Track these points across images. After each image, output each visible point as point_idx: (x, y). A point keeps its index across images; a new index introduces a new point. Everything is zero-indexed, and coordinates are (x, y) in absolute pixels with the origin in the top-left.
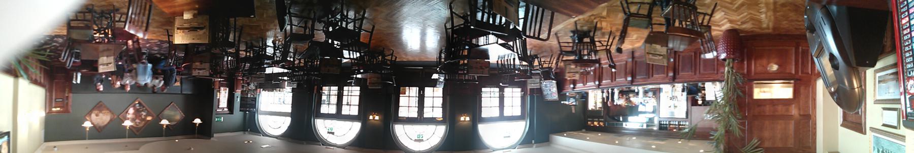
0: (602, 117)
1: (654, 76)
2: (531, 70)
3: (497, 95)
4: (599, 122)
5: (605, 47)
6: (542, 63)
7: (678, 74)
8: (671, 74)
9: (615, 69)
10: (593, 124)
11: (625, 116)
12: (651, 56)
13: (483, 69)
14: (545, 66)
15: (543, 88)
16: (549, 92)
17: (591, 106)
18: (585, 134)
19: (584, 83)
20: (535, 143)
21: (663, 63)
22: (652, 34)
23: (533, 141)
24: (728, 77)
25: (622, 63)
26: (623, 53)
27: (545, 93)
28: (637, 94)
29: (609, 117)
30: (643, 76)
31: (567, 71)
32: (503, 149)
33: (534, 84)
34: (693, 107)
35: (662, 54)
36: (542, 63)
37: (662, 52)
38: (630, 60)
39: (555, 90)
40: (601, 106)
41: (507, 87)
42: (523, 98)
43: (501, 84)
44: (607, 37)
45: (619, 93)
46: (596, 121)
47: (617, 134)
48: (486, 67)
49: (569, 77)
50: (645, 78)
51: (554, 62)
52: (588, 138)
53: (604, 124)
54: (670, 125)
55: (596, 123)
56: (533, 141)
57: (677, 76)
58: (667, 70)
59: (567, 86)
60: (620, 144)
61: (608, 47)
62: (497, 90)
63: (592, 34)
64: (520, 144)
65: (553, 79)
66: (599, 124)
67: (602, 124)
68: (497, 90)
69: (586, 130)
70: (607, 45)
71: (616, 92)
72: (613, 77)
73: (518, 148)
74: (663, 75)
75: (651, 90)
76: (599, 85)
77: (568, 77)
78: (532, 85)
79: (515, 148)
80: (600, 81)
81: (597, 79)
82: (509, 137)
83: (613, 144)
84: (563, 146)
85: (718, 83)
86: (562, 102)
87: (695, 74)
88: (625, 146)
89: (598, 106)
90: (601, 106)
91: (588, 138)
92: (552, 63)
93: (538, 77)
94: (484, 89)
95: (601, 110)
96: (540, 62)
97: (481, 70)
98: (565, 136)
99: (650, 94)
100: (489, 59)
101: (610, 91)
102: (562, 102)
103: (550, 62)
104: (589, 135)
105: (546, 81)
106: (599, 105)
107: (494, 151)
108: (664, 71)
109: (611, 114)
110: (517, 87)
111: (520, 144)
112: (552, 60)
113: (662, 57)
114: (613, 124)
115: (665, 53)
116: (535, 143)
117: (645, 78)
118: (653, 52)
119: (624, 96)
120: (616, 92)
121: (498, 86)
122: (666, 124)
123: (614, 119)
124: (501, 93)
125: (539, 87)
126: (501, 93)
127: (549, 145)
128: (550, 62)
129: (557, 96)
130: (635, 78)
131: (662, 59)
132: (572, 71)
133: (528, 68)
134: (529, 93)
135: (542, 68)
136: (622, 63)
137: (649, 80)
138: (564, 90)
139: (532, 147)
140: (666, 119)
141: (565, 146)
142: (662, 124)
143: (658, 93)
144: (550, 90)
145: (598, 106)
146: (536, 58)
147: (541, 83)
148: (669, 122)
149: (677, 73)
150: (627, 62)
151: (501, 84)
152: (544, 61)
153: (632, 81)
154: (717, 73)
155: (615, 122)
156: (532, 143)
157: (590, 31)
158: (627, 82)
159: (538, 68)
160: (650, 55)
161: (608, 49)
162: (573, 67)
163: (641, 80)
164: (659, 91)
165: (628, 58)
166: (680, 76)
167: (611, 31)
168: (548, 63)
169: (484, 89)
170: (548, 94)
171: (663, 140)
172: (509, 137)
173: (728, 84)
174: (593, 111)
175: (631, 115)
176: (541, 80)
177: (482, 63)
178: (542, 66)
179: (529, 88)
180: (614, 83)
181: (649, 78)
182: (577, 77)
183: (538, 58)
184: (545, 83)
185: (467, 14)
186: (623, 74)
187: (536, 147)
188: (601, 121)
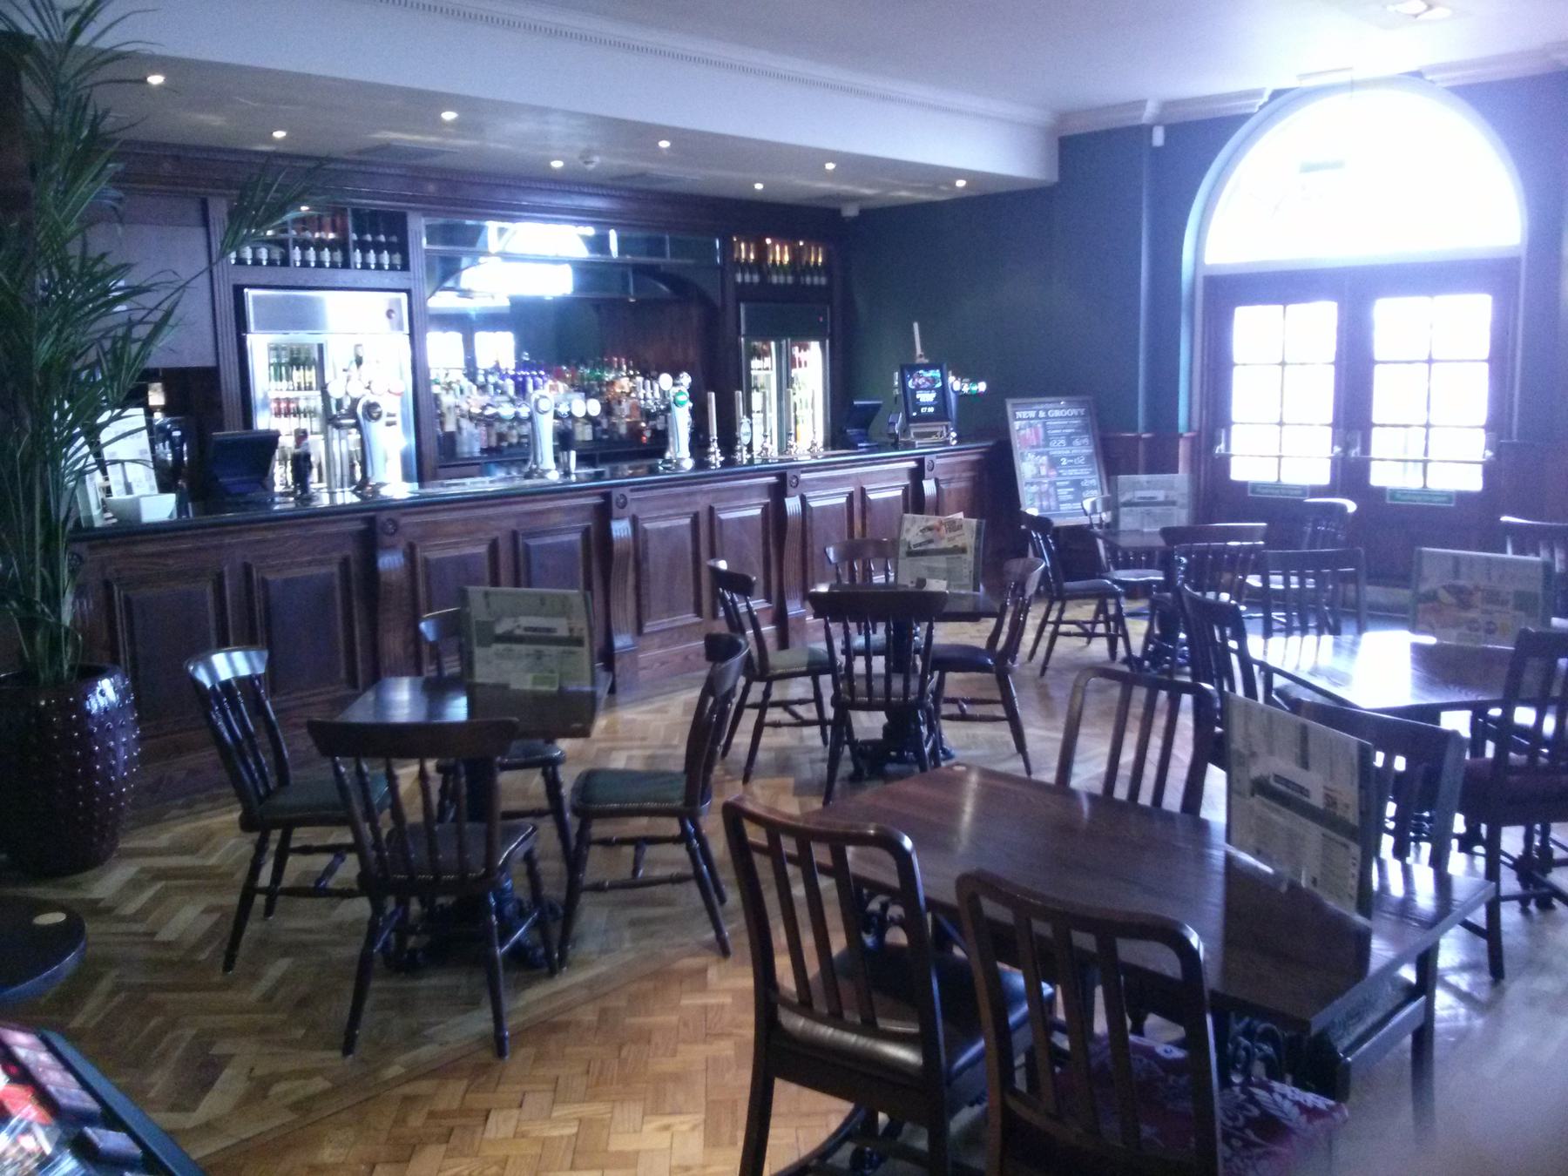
0: (744, 293)
1: (482, 549)
2: (1168, 584)
3: (1381, 442)
4: (761, 265)
5: (776, 695)
6: (1101, 628)
7: (345, 563)
8: (390, 562)
9: (715, 571)
10: (796, 254)
11: (612, 302)
12: (561, 627)
13: (1448, 589)
14: (1084, 611)
15: (1091, 478)
16: (1059, 449)
17: (812, 362)
18: (846, 188)
19: (859, 503)
20: (1148, 130)
21: (486, 594)
22: (578, 725)
23: (1158, 138)
24: (52, 564)
25: (666, 622)
26: (704, 635)
27: (1084, 447)
28: (564, 439)
29: (704, 300)
30: (542, 548)
31: (969, 557)
32: (1353, 85)
33: (1151, 502)
34: (209, 362)
35: (500, 647)
36: (1101, 628)
37: (499, 655)
38: (621, 641)
39: (1028, 467)
40: (755, 363)
41: (1316, 491)
42: (1216, 417)
43: (1351, 507)
44: (761, 756)
45: (661, 440)
46: (780, 269)
47: (659, 187)
48: (1432, 597)
49: (954, 527)
50: (533, 534)
51: (1028, 637)
52: (830, 166)
53: (728, 248)
54: (341, 245)
55: (781, 255)
56: (1158, 138)
57: (351, 551)
58: (414, 591)
59: (963, 484)
60: (645, 133)
61: (756, 694)
62: (1381, 476)
63: (846, 767)
64: (1244, 118)
65: (1042, 524)
66: (762, 251)
67: (746, 253)
68: (1381, 476)
69: (836, 213)
70: (763, 707)
71: (680, 450)
72: (706, 531)
73: (1257, 93)
74: (434, 555)
75: (476, 466)
76: (779, 492)
77: (965, 529)
78: (1160, 495)
79: (1276, 94)
80: (775, 515)
81: (793, 527)
82: (1308, 169)
83: (684, 131)
84: (979, 116)
85: (99, 519)
86: (982, 387)
87: (247, 569)
88: (588, 116)
89: (770, 362)
90: (755, 363)
91: (830, 166)
92: (1044, 622)
93: (1124, 541)
94: (1473, 481)
95: (752, 334)
96: (1117, 631)
97: (1461, 582)
98: (960, 173)
99: (473, 440)
100: (1418, 649)
101: (716, 458)
102: (982, 387)
103: (1055, 635)
104: (823, 183)
105: (1084, 520)
106: (763, 369)
107: (1418, 74)
108: (428, 577)
109: (695, 312)
110: (1255, 487)
111: (1244, 118)
112: (1044, 644)
113: (500, 629)
114: (680, 248)
115: (479, 652)
116: (1148, 130)
117: (533, 534)
118: (554, 650)
119: (623, 430)
120: (680, 450)
121: (1372, 498)
122: (364, 247)
123: (679, 284)
124: (1355, 452)
125: (1122, 478)
126: (1355, 452)
127: (1063, 117)
128: (1055, 635)
129: (1017, 425)
130: (586, 532)
131: (499, 619)
132: (940, 562)
133: (1390, 875)
134: (1183, 449)
135: (1102, 595)
136: (666, 622)
137: (511, 524)
138: (977, 462)
139: (1167, 105)
140: (304, 276)
141: (960, 113)
142: (392, 249)
143: (431, 447)
144: (1054, 463)
145: (770, 362)
146: (1139, 661)
147: (1111, 504)
148: (346, 264)
149: (354, 568)
150: (639, 630)
151: (1351, 507)
152: (1090, 636)
153: (604, 513)
154: (107, 585)
155: (667, 260)
156: (1170, 130)
157: (856, 779)
158: (632, 508)
159: (1127, 606)
160: (563, 632)
161: (760, 679)
162: (936, 585)
163: (556, 518)
164: (429, 463)
165: (632, 653)
166: (337, 556)
167: (746, 780)
168: (1063, 628)
169: (1473, 481)
170: (1069, 442)
171: (386, 148)
172: (1308, 169)
173: (46, 518)
174: (802, 335)
175: (563, 308)
176: (1112, 528)
177: (1456, 624)
178: (1102, 609)
179: (1181, 479)
180: (701, 504)
181: (514, 535)
182: (913, 529)
183: (1129, 659)
184: (1087, 505)
185: (1525, 911)
186: (657, 555)
187: (1141, 104)
188: (746, 267)
